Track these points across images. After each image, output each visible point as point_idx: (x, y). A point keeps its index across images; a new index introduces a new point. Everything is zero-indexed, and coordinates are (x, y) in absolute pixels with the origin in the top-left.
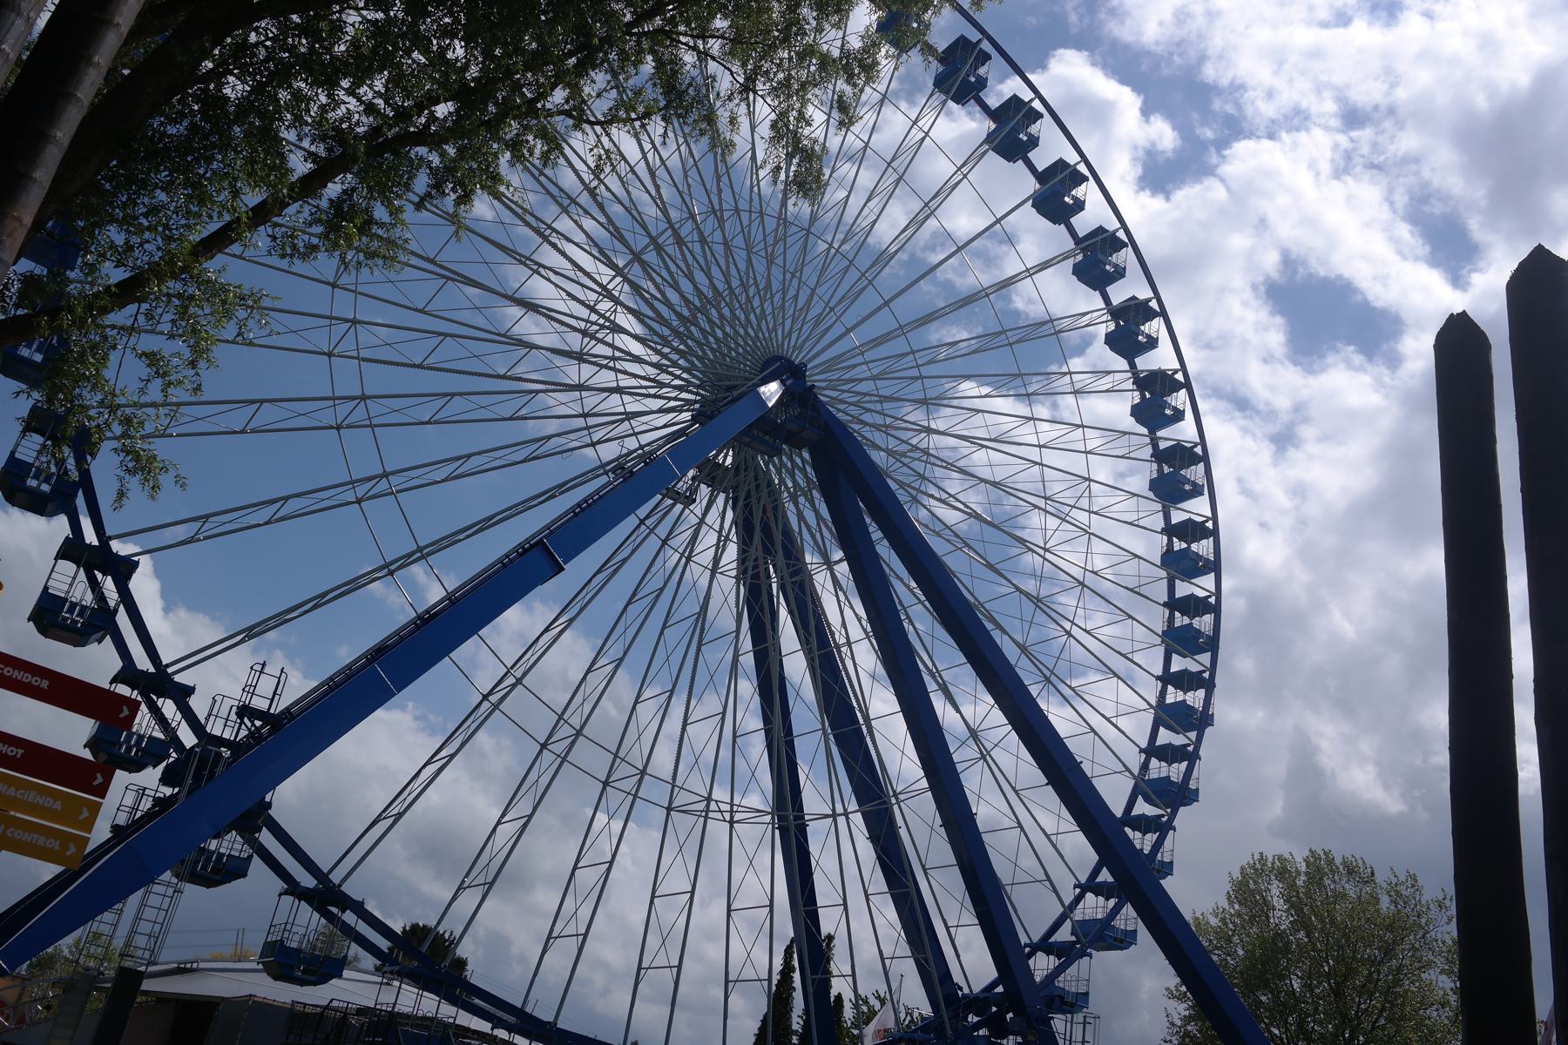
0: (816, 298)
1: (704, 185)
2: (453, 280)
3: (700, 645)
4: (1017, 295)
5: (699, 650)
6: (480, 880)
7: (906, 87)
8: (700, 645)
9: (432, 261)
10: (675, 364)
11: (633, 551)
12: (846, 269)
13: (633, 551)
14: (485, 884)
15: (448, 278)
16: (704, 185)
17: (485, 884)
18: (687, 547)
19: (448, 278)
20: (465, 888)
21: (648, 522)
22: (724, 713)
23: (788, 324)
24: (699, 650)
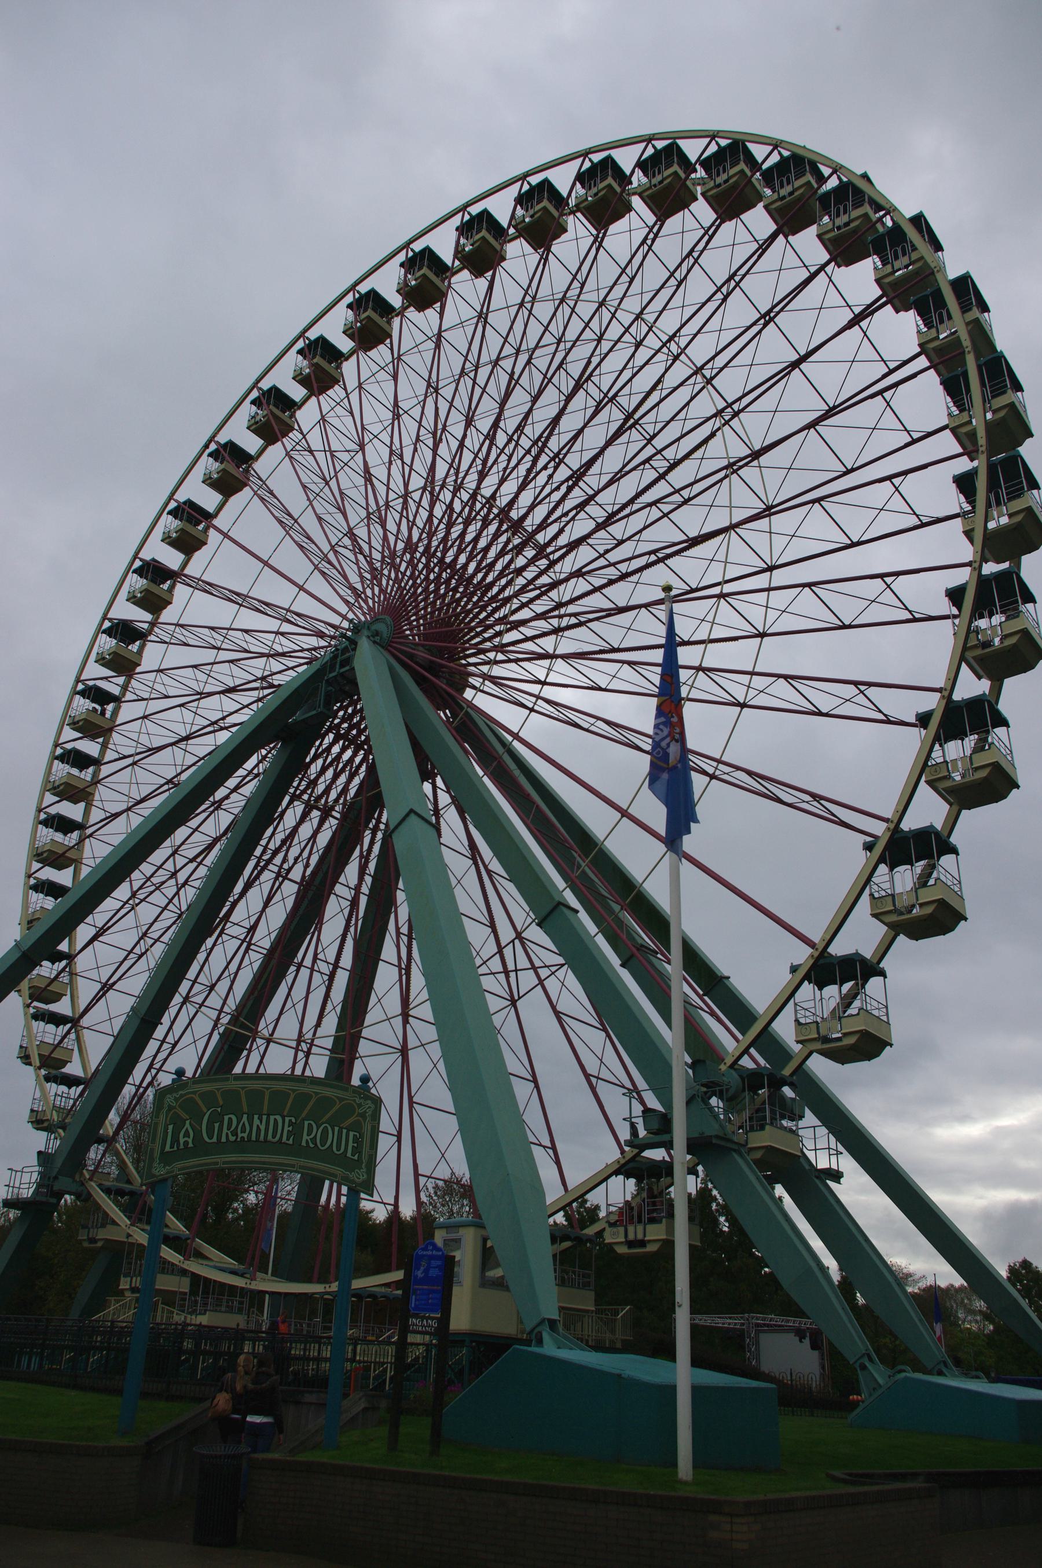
0: (546, 663)
1: (682, 326)
2: (410, 1098)
3: (693, 591)
4: (690, 1195)
5: (697, 590)
6: (861, 699)
7: (986, 613)
8: (693, 591)
9: (399, 1136)
10: (412, 525)
11: (738, 768)
12: (283, 634)
13: (738, 768)
14: (862, 692)
15: (411, 1103)
16: (682, 326)
17: (862, 692)
18: (290, 657)
19: (411, 1103)
20: (885, 715)
21: (711, 770)
22: (818, 500)
23: (525, 614)
24: (697, 590)
